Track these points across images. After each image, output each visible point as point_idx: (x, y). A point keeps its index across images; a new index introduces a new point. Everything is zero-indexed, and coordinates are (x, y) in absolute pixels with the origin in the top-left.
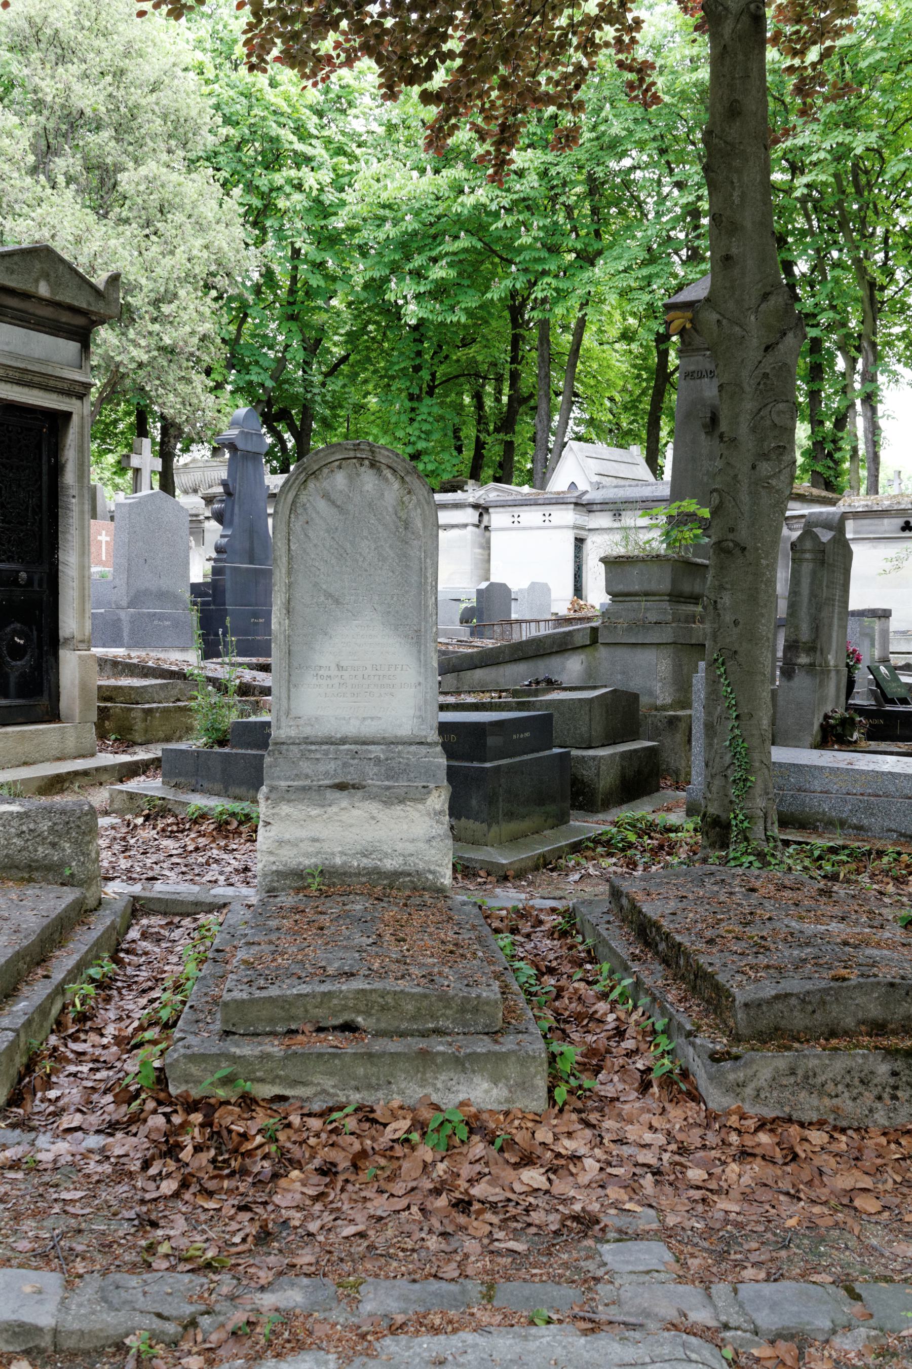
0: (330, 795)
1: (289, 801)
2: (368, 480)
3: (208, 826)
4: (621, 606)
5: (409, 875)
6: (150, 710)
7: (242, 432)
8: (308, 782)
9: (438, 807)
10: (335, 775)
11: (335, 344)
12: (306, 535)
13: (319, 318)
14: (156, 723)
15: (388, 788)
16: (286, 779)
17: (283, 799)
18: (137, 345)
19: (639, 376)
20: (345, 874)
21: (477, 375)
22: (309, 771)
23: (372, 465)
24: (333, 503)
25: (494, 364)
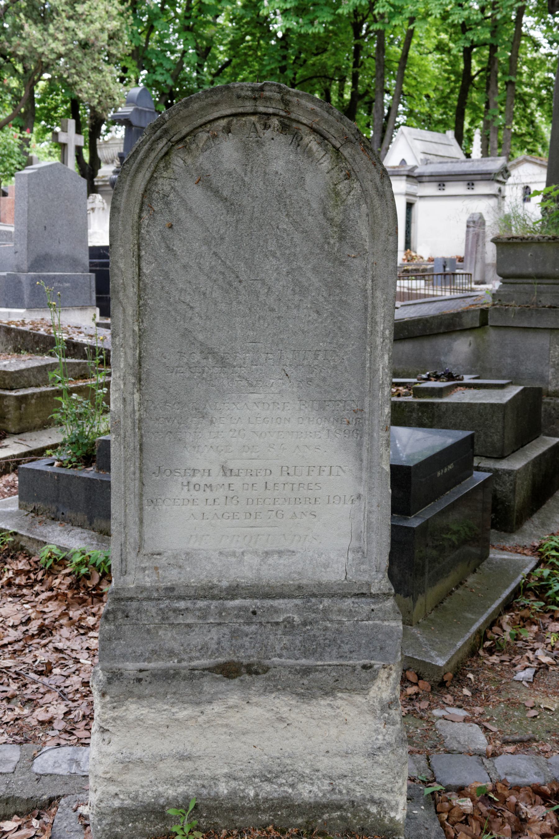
0: (209, 686)
1: (140, 697)
2: (278, 153)
3: (61, 582)
4: (511, 289)
5: (339, 807)
6: (25, 397)
7: (136, 110)
8: (173, 663)
9: (386, 695)
10: (219, 650)
11: (221, 52)
12: (169, 249)
13: (208, 31)
14: (32, 409)
15: (306, 671)
16: (137, 658)
17: (131, 694)
18: (56, 39)
19: (448, 79)
20: (234, 809)
21: (326, 77)
22: (176, 646)
23: (285, 128)
24: (216, 192)
25: (338, 69)
